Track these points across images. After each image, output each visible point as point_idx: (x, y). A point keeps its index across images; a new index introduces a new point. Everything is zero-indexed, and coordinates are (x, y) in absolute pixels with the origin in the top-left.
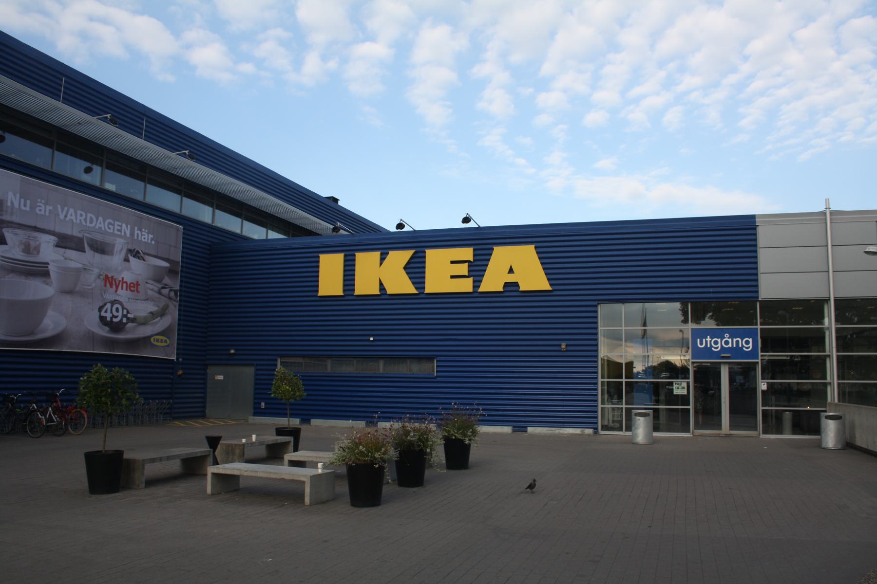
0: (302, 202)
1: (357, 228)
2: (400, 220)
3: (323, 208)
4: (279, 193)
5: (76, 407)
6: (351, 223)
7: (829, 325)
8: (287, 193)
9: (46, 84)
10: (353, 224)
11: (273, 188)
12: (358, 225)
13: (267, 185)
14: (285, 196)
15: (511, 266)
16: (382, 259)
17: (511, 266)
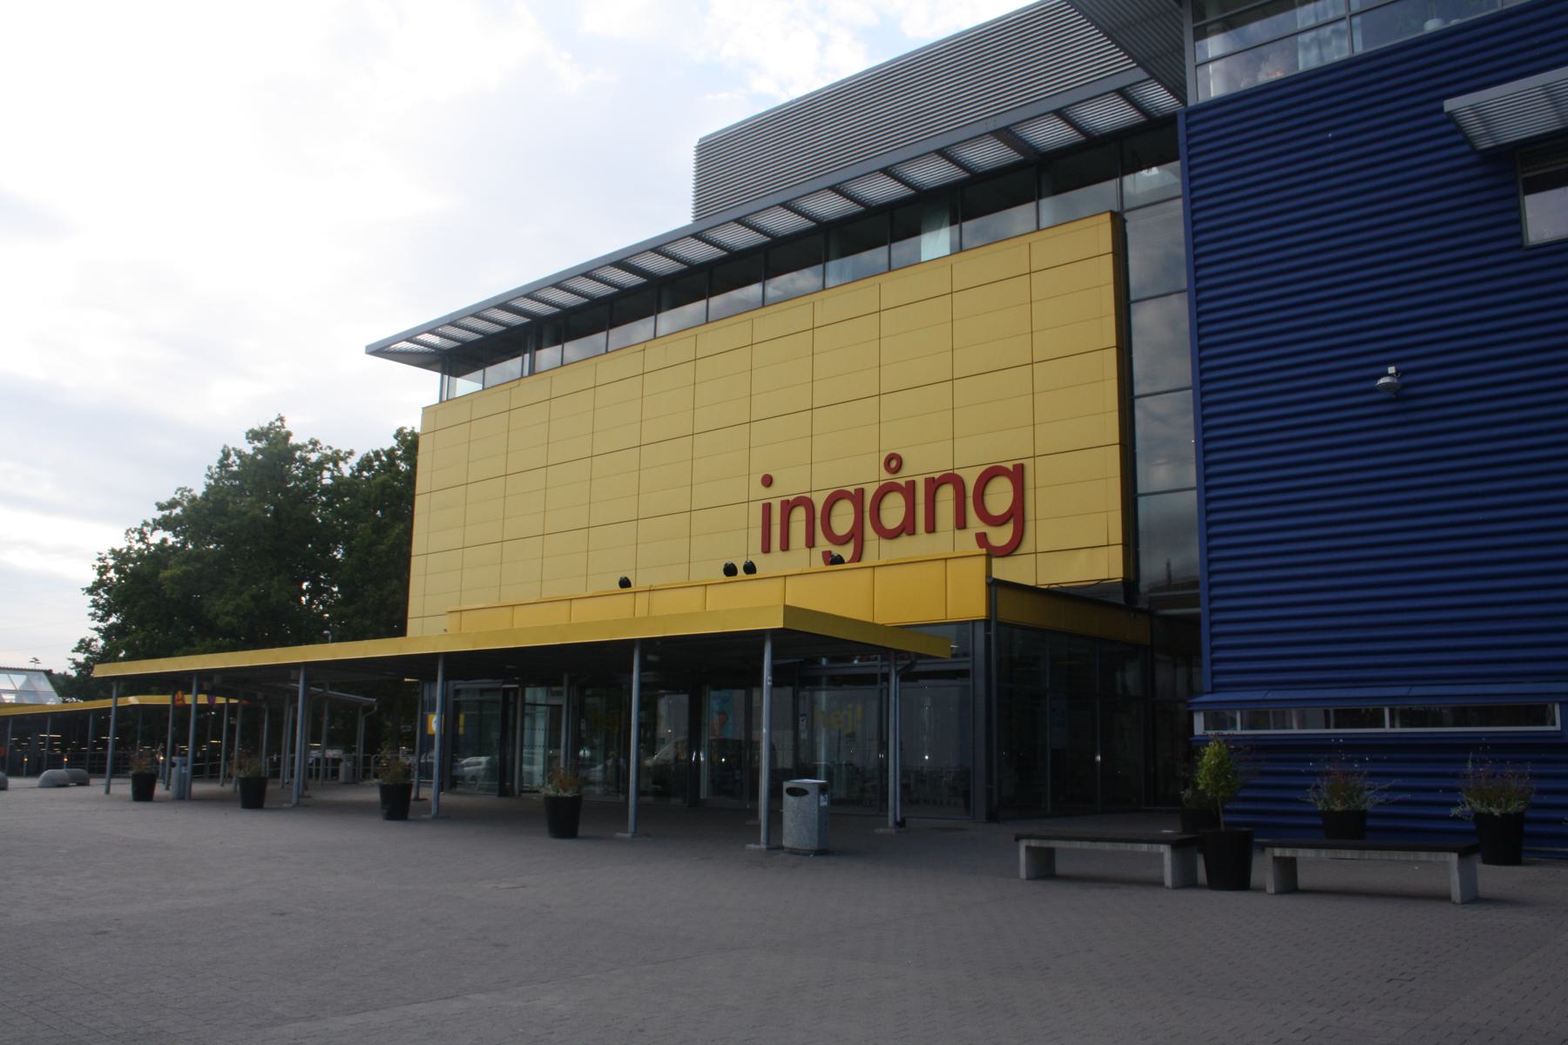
0: (875, 131)
1: (1067, 47)
2: (276, 417)
3: (1365, 223)
4: (863, 106)
5: (321, 448)
6: (972, 46)
7: (991, 562)
8: (1011, 41)
9: (1098, 44)
10: (869, 86)
11: (986, 67)
12: (1018, 65)
13: (999, 43)
14: (950, 64)
15: (381, 351)
16: (1168, 565)
17: (381, 351)
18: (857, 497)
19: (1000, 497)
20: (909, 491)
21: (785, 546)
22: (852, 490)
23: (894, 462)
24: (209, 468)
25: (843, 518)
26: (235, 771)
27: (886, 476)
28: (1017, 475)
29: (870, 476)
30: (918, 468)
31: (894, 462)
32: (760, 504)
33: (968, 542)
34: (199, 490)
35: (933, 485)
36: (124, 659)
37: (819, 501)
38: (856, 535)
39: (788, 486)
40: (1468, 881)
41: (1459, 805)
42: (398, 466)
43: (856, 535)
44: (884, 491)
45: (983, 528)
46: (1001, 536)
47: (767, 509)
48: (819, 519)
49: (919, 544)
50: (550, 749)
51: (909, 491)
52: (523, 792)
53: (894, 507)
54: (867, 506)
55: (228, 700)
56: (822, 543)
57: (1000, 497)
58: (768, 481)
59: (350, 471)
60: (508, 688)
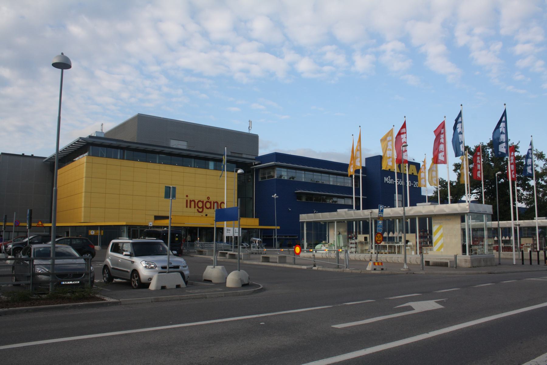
18: (203, 202)
19: (200, 205)
20: (210, 203)
21: (190, 207)
22: (202, 201)
23: (208, 198)
24: (513, 143)
26: (396, 234)
27: (207, 200)
29: (205, 200)
30: (212, 199)
31: (208, 198)
32: (186, 200)
34: (526, 154)
35: (214, 203)
36: (177, 165)
37: (196, 201)
38: (203, 207)
39: (191, 197)
42: (502, 182)
43: (203, 207)
44: (207, 202)
45: (198, 208)
47: (187, 201)
48: (197, 204)
50: (347, 222)
51: (210, 203)
52: (170, 255)
53: (208, 205)
55: (53, 262)
56: (197, 208)
58: (187, 196)
60: (197, 230)
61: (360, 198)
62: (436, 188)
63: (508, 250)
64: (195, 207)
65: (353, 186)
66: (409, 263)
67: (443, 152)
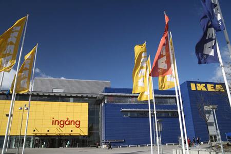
18: (64, 121)
19: (78, 123)
21: (55, 124)
23: (68, 119)
25: (62, 123)
28: (79, 121)
29: (65, 120)
30: (70, 119)
33: (59, 126)
35: (71, 121)
37: (59, 121)
38: (63, 124)
40: (206, 87)
41: (92, 125)
43: (63, 124)
46: (78, 126)
48: (59, 122)
49: (70, 126)
51: (69, 121)
53: (67, 123)
54: (65, 122)
57: (78, 123)
59: (15, 39)
61: (151, 109)
62: (208, 11)
63: (7, 97)
64: (74, 124)
65: (176, 103)
66: (211, 90)
67: (13, 46)
